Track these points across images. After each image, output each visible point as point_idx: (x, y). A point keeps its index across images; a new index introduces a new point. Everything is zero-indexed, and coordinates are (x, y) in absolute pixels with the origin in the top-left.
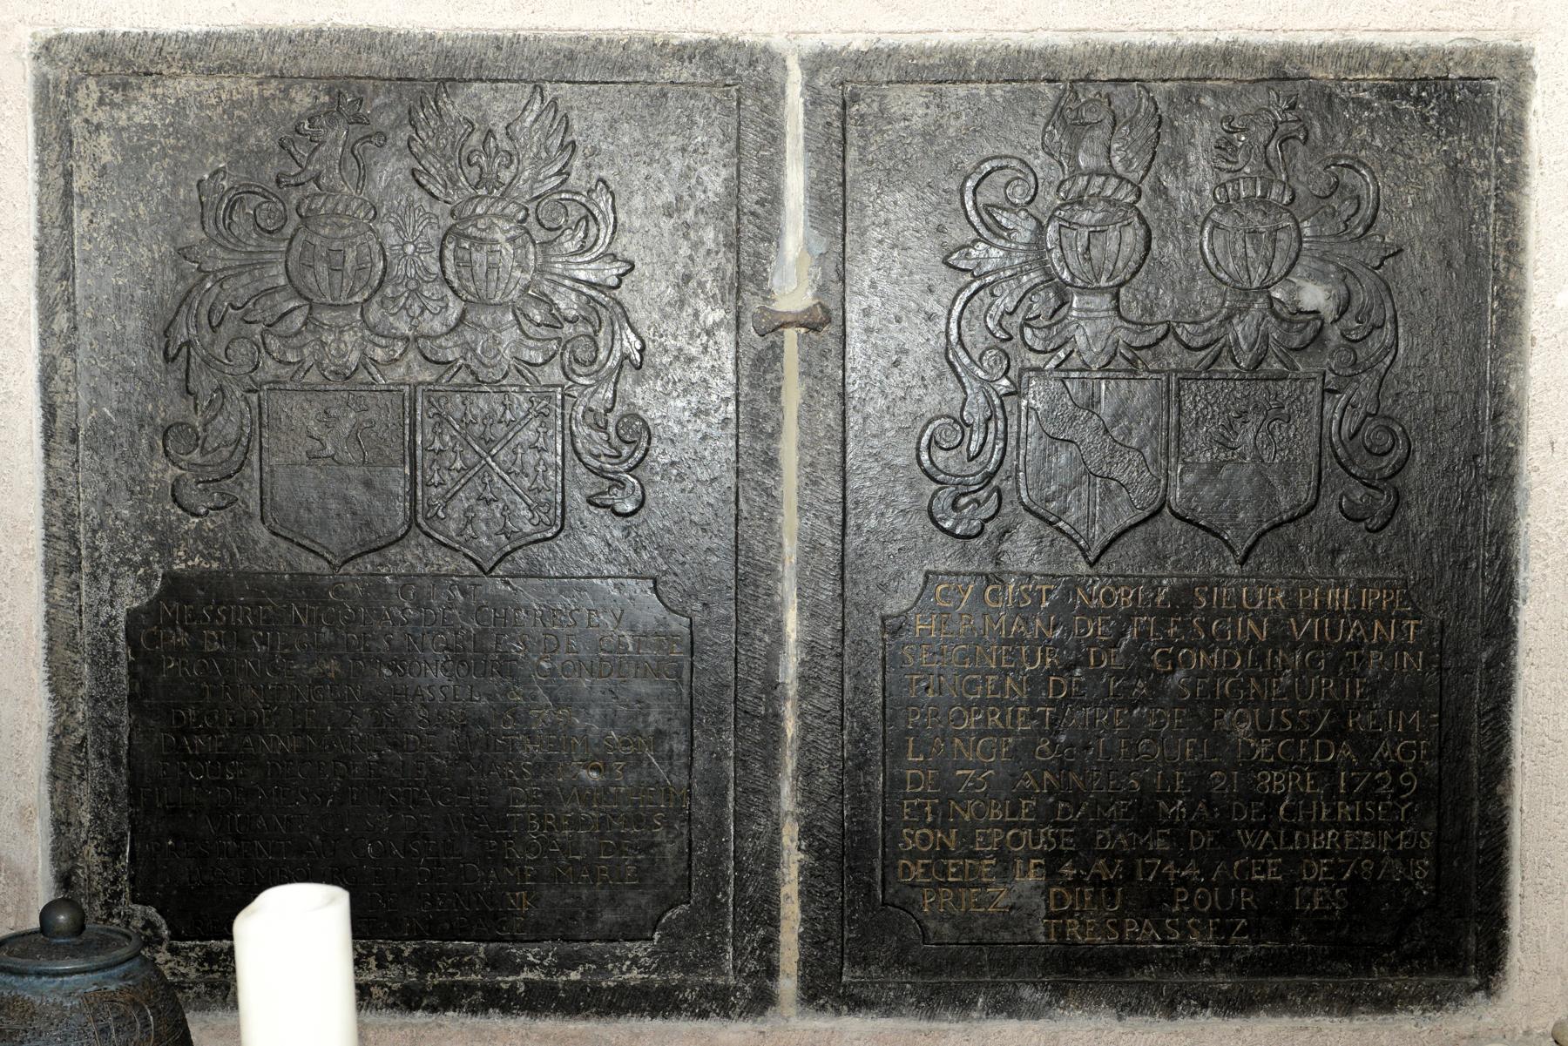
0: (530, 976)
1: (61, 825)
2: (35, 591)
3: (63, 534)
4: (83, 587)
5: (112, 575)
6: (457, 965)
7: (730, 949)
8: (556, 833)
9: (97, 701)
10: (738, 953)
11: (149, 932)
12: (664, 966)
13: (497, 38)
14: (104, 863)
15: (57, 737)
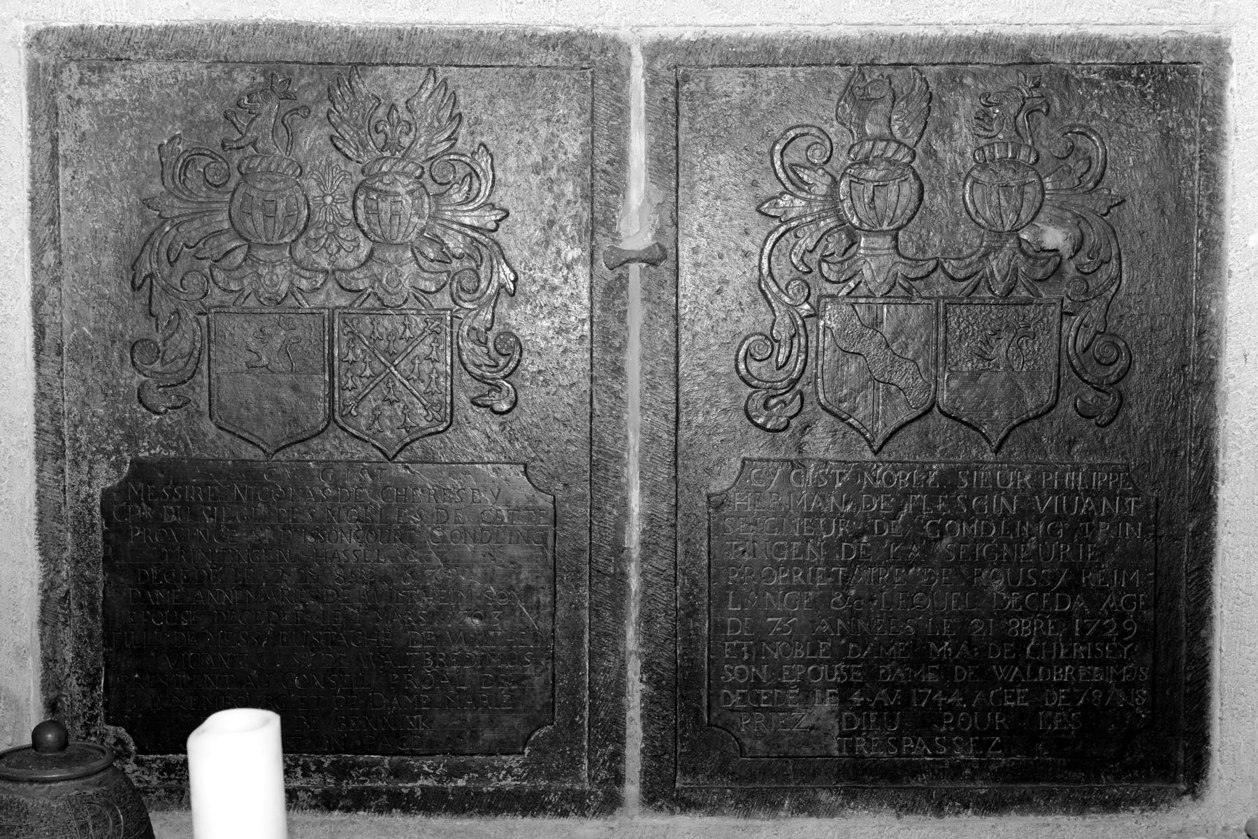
0: (425, 783)
1: (49, 662)
2: (28, 474)
3: (50, 428)
4: (67, 471)
5: (90, 461)
6: (367, 774)
7: (586, 761)
9: (78, 562)
10: (592, 764)
11: (119, 748)
12: (532, 775)
13: (399, 31)
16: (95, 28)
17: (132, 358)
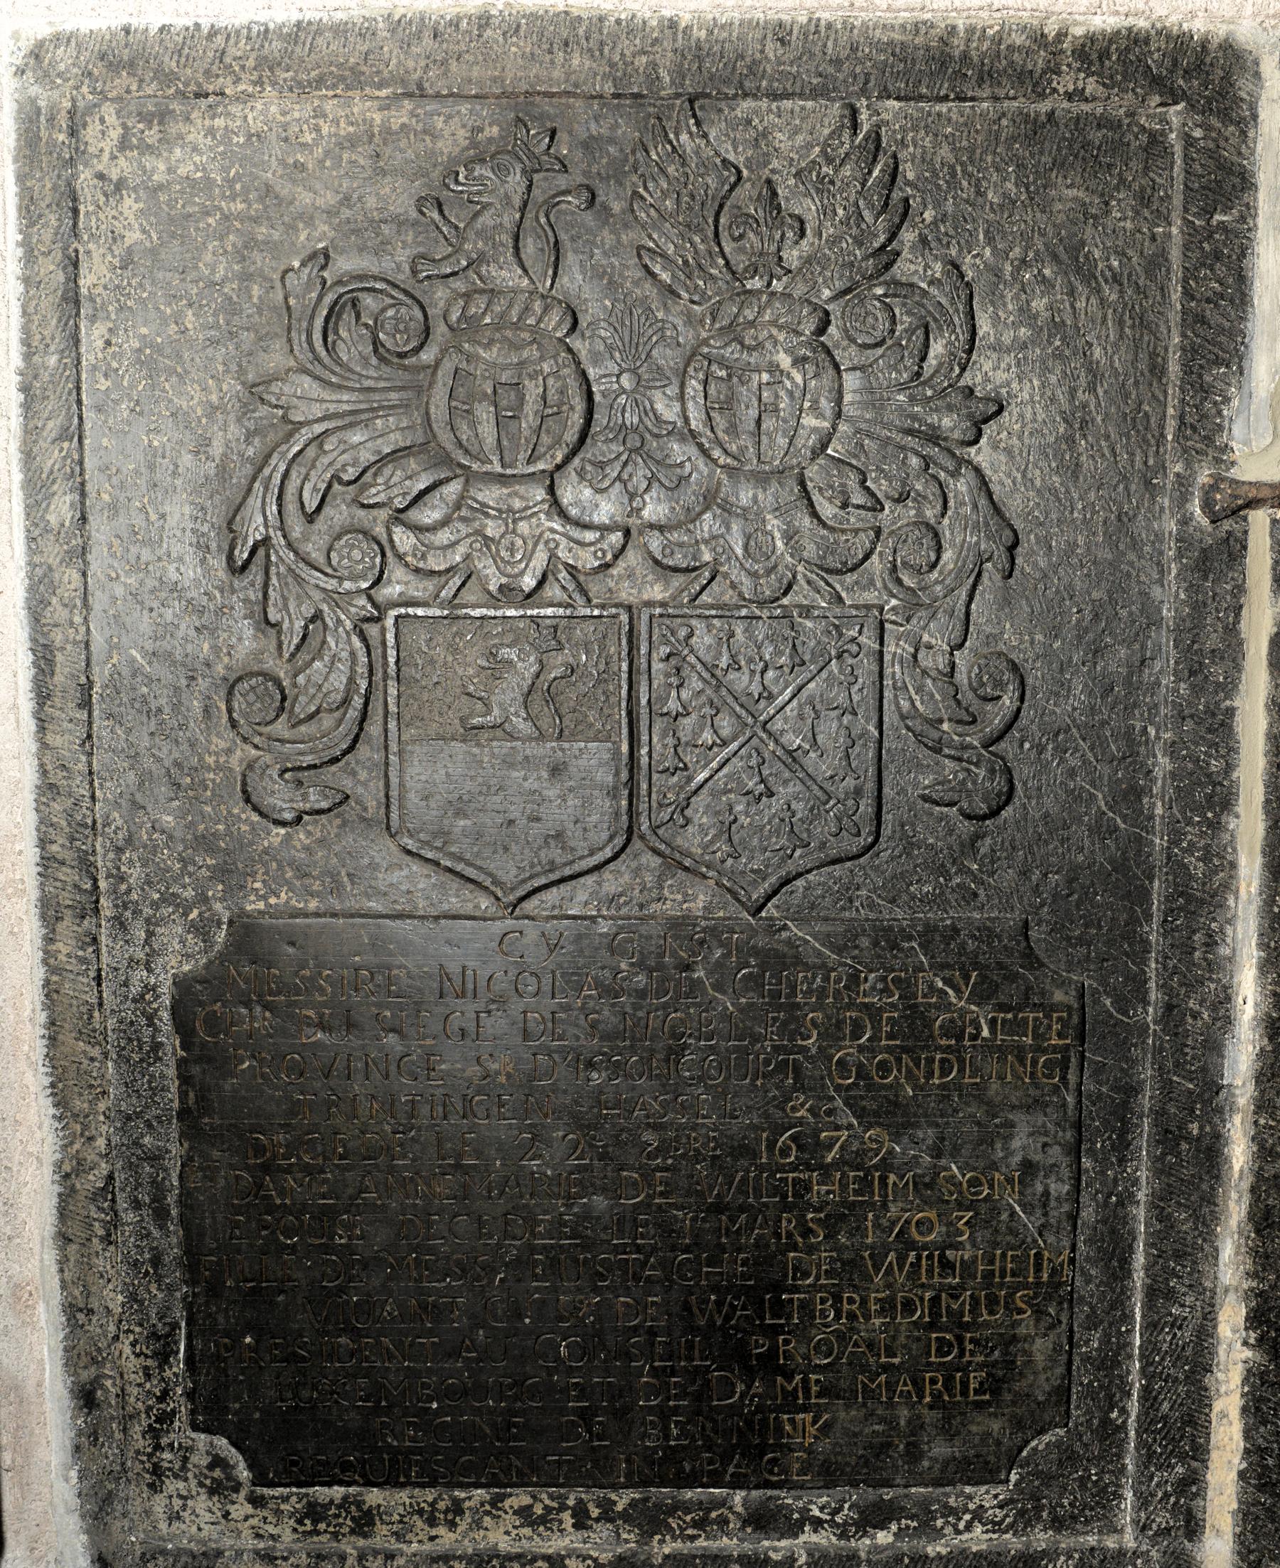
0: (814, 1538)
1: (76, 1312)
2: (27, 948)
3: (68, 855)
4: (104, 939)
5: (148, 921)
6: (700, 1524)
7: (1129, 1495)
8: (861, 1323)
9: (129, 1118)
10: (1143, 1501)
11: (217, 1473)
12: (1025, 1520)
13: (780, 24)
14: (146, 1368)
15: (67, 1176)
16: (153, 30)
17: (230, 711)
